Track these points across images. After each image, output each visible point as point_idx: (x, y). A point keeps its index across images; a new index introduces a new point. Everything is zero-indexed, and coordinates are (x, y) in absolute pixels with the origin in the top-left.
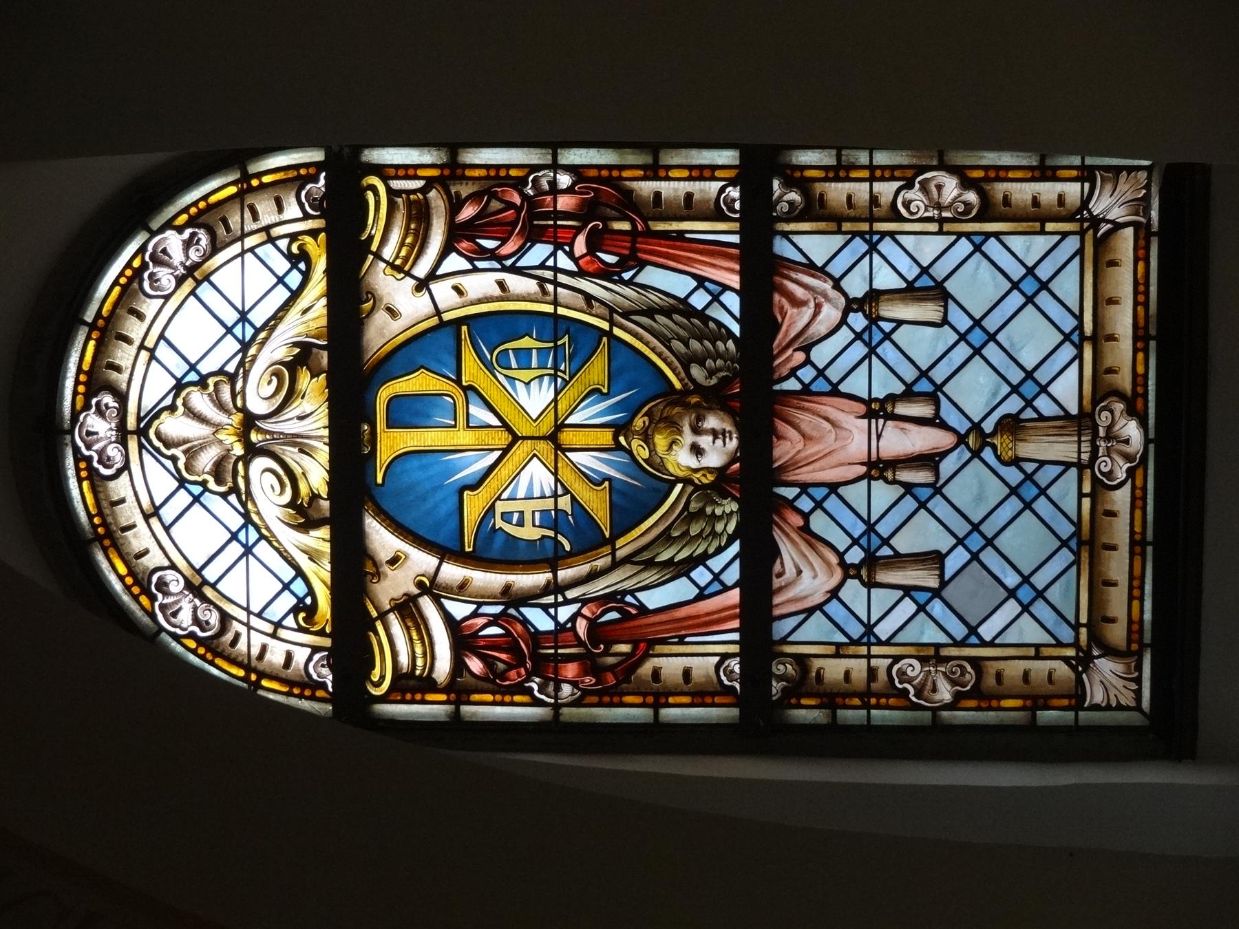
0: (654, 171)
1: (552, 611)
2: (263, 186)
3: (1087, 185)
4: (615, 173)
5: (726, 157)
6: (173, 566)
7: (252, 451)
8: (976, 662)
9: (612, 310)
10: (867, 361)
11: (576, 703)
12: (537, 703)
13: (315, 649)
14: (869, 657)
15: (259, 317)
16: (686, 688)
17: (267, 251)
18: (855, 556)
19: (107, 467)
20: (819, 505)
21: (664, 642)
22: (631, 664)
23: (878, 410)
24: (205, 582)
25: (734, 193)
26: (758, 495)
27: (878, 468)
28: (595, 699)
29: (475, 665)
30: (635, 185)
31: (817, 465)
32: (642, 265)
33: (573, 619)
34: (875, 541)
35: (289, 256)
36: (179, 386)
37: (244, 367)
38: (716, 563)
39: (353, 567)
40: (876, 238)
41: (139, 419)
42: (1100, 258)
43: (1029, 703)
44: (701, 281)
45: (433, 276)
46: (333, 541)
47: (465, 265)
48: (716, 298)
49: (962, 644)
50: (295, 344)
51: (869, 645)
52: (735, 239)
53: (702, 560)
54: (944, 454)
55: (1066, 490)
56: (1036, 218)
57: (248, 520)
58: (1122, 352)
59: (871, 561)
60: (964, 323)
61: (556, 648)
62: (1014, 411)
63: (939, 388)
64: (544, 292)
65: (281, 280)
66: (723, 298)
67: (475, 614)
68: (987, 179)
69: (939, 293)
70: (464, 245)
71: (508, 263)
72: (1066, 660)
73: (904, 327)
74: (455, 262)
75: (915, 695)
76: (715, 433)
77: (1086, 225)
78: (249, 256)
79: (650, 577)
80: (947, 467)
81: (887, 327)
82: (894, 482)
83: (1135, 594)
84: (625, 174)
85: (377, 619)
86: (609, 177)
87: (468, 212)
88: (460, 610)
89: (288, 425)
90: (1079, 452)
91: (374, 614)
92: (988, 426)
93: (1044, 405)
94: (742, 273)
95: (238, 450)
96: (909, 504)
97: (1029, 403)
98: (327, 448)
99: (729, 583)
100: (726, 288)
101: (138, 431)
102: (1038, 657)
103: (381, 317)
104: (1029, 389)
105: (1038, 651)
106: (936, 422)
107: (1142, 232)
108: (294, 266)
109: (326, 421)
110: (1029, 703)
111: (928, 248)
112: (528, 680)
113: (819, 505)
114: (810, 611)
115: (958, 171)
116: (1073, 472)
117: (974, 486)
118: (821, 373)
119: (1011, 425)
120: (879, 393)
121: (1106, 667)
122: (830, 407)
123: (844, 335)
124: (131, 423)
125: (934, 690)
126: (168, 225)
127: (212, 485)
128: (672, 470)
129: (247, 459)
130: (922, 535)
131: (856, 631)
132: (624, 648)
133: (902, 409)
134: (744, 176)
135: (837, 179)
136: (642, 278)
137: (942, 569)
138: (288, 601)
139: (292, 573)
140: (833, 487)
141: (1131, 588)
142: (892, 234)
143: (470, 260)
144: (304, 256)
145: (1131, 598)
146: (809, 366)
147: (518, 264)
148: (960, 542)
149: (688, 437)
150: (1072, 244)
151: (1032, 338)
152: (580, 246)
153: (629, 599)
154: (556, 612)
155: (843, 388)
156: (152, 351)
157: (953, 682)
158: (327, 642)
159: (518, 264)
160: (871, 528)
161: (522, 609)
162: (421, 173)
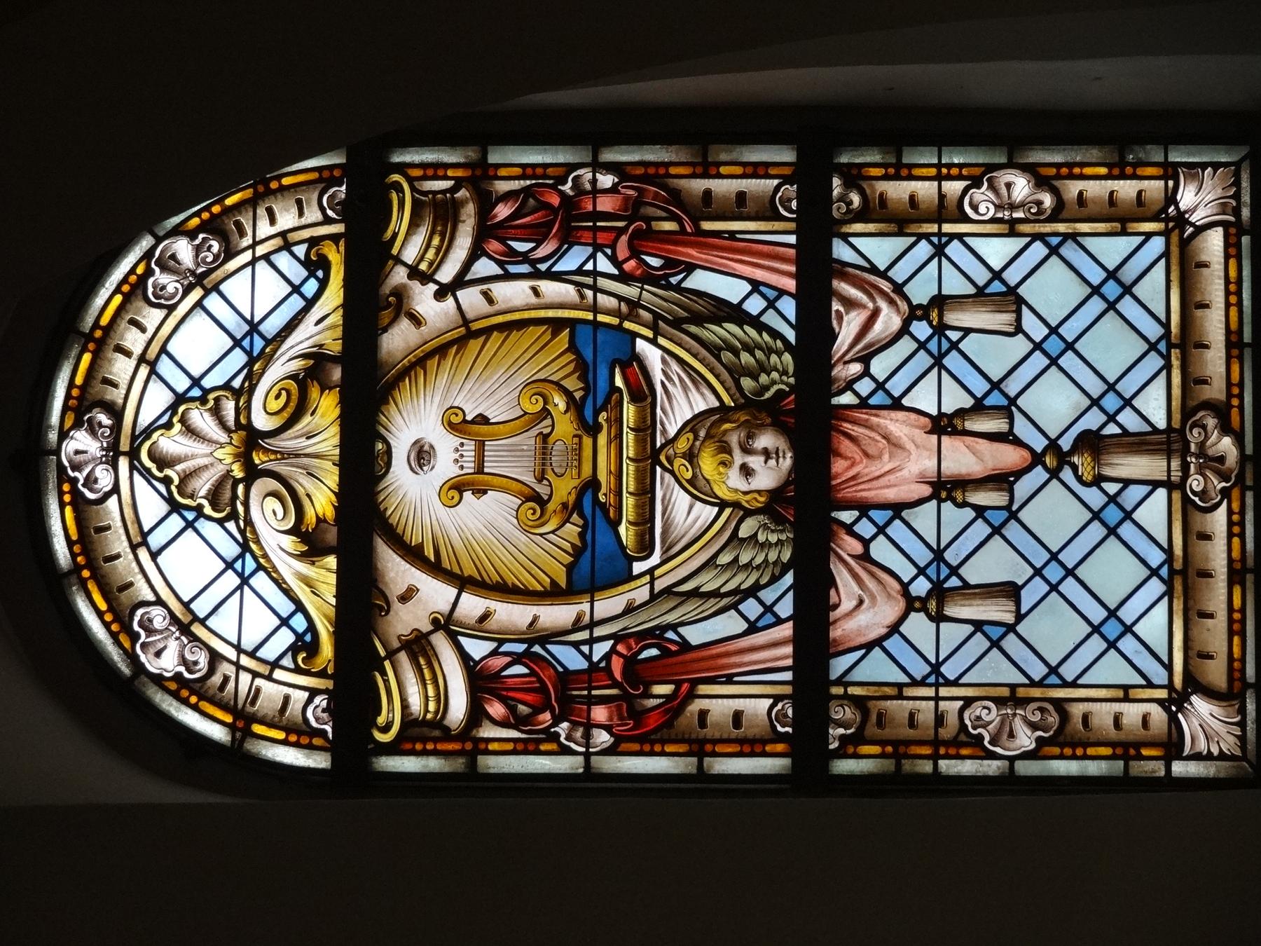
0: (707, 169)
1: (585, 649)
2: (282, 189)
3: (1171, 183)
4: (662, 171)
5: (786, 155)
6: (160, 602)
7: (253, 474)
8: (1059, 704)
9: (657, 317)
11: (610, 751)
13: (313, 692)
14: (937, 699)
15: (271, 327)
16: (735, 733)
17: (283, 260)
18: (921, 587)
19: (91, 490)
22: (676, 705)
23: (943, 425)
24: (195, 619)
25: (791, 190)
26: (810, 515)
30: (683, 183)
32: (690, 268)
33: (607, 657)
36: (180, 399)
37: (252, 380)
38: (768, 595)
39: (361, 600)
40: (932, 679)
41: (134, 437)
42: (1186, 268)
43: (1119, 751)
44: (756, 285)
45: (460, 281)
46: (341, 573)
47: (494, 269)
48: (771, 304)
49: (1040, 684)
50: (304, 356)
51: (937, 685)
52: (792, 239)
53: (753, 591)
55: (1154, 511)
56: (1120, 218)
57: (245, 547)
58: (1214, 361)
59: (939, 592)
60: (1037, 331)
61: (590, 689)
63: (1013, 401)
64: (582, 297)
65: (296, 289)
66: (779, 304)
67: (494, 653)
69: (1012, 300)
70: (494, 246)
72: (1159, 701)
74: (484, 267)
76: (766, 453)
77: (1171, 225)
78: (262, 267)
79: (690, 609)
80: (1023, 487)
81: (954, 336)
84: (673, 171)
85: (385, 659)
86: (655, 175)
87: (503, 211)
88: (477, 649)
90: (1169, 471)
91: (382, 653)
92: (1066, 443)
93: (1128, 419)
94: (797, 276)
95: (238, 473)
96: (981, 530)
97: (1112, 418)
98: (336, 470)
99: (783, 616)
100: (782, 292)
101: (126, 447)
102: (1126, 699)
104: (1111, 402)
105: (1126, 693)
108: (312, 274)
109: (336, 440)
111: (997, 251)
113: (881, 530)
114: (869, 647)
116: (1161, 493)
117: (1054, 511)
118: (880, 386)
119: (1091, 442)
120: (948, 408)
121: (1200, 705)
122: (895, 424)
124: (125, 445)
125: (1012, 735)
126: (177, 231)
127: (208, 510)
128: (719, 493)
129: (249, 480)
130: (994, 564)
132: (664, 689)
133: (971, 425)
136: (691, 283)
137: (1018, 604)
138: (285, 638)
139: (292, 607)
140: (898, 509)
141: (1231, 621)
142: (960, 237)
143: (500, 264)
144: (324, 264)
146: (867, 379)
147: (555, 269)
148: (1038, 572)
149: (739, 458)
150: (1157, 244)
151: (1112, 348)
152: (622, 251)
153: (670, 635)
155: (905, 402)
156: (153, 365)
157: (1034, 726)
158: (329, 684)
159: (555, 269)
160: (938, 555)
162: (450, 173)
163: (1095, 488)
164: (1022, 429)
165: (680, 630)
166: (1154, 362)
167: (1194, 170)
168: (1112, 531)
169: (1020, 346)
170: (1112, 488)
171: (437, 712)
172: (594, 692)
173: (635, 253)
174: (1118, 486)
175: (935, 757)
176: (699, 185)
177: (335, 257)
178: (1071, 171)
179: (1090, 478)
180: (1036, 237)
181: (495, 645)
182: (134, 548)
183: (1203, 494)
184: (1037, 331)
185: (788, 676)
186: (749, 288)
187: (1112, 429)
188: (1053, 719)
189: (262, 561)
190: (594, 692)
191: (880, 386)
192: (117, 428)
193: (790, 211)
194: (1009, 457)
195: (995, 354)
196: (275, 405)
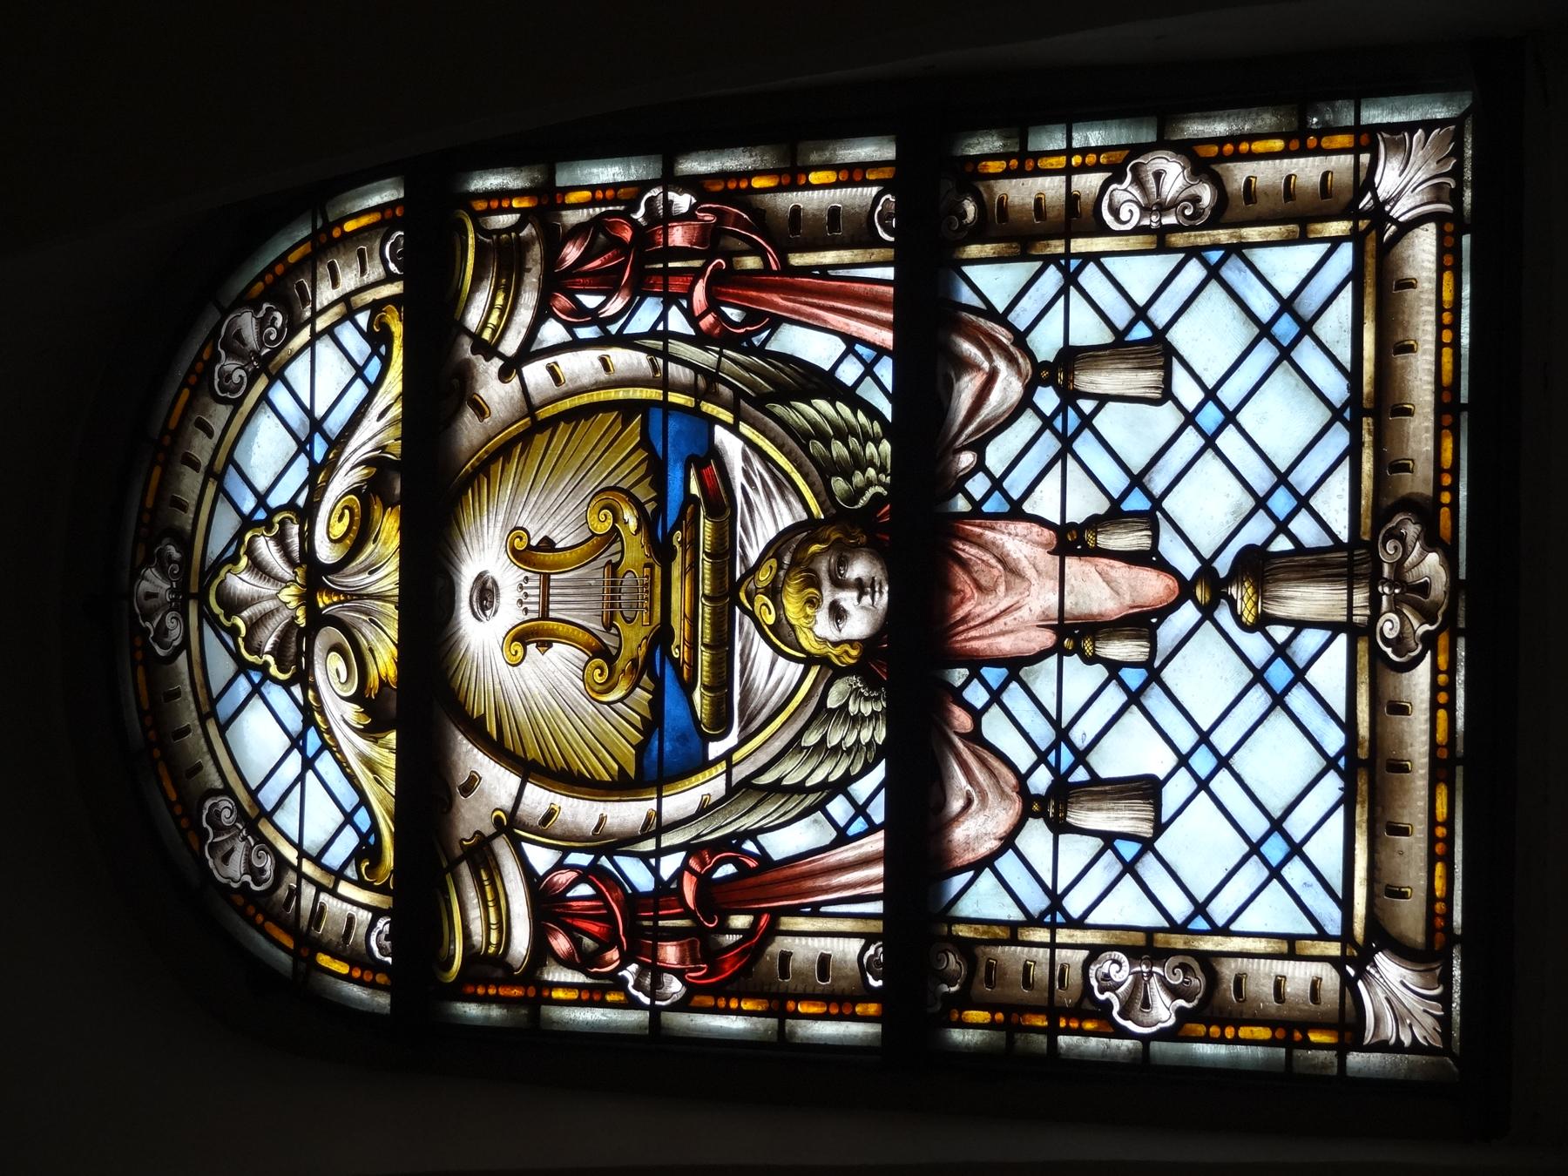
8: (1208, 960)
10: (1059, 465)
11: (683, 1005)
12: (633, 1004)
14: (1053, 946)
18: (1041, 781)
20: (996, 697)
21: (795, 911)
23: (1071, 541)
27: (1074, 634)
28: (709, 1001)
29: (561, 944)
31: (990, 629)
32: (775, 323)
33: (678, 876)
34: (1067, 758)
35: (368, 335)
38: (861, 789)
39: (426, 790)
40: (1074, 263)
44: (850, 341)
45: (528, 353)
46: (401, 752)
48: (869, 370)
51: (1053, 927)
52: (888, 273)
53: (840, 787)
54: (1165, 612)
56: (1298, 216)
57: (308, 722)
62: (1258, 540)
63: (1157, 503)
68: (1222, 158)
69: (1159, 352)
71: (613, 329)
73: (1111, 406)
75: (1120, 1014)
76: (860, 587)
77: (1363, 224)
80: (1169, 631)
81: (1087, 406)
82: (1090, 660)
83: (1438, 853)
88: (541, 858)
89: (356, 580)
92: (1223, 566)
94: (894, 326)
97: (1282, 527)
98: (395, 614)
100: (881, 351)
103: (469, 415)
105: (1290, 946)
106: (1150, 559)
107: (1449, 228)
110: (1280, 1034)
111: (1141, 274)
112: (623, 966)
115: (1186, 150)
117: (1206, 671)
119: (1257, 566)
120: (1077, 514)
121: (1390, 971)
123: (1027, 425)
127: (274, 670)
130: (1131, 751)
131: (1037, 902)
132: (741, 921)
134: (899, 179)
135: (1020, 173)
141: (1432, 839)
143: (569, 327)
145: (1432, 859)
151: (1284, 419)
153: (749, 846)
154: (658, 862)
157: (1174, 992)
161: (619, 860)
163: (1258, 634)
166: (1339, 439)
168: (1278, 700)
169: (1166, 419)
170: (1280, 633)
172: (661, 923)
173: (713, 304)
174: (1288, 630)
179: (1251, 619)
185: (877, 907)
187: (1282, 544)
188: (1198, 982)
190: (661, 923)
191: (997, 484)
193: (887, 230)
196: (339, 529)
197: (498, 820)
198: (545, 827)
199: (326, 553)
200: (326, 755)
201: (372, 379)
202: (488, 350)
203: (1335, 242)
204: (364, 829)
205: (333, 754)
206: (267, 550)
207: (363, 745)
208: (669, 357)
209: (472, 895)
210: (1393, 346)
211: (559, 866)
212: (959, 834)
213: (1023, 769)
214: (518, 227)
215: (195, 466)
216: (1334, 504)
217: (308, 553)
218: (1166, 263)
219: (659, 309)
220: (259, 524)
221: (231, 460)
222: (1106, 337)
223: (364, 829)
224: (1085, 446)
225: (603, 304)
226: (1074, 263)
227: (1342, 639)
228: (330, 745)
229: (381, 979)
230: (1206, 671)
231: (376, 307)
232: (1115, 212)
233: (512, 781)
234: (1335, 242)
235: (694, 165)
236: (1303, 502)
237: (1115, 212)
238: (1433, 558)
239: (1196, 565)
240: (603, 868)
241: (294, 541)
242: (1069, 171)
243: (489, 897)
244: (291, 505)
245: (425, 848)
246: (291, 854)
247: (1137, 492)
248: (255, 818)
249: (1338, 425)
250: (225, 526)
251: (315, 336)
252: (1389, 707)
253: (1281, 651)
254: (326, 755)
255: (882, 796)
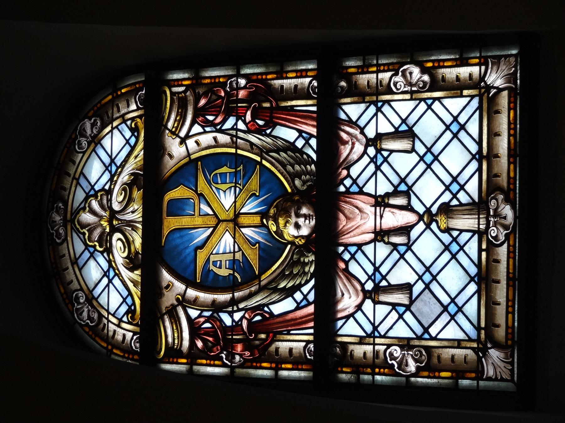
0: (281, 75)
3: (483, 68)
8: (428, 349)
11: (242, 366)
18: (369, 286)
20: (353, 257)
23: (381, 202)
27: (380, 235)
35: (131, 129)
38: (305, 289)
44: (300, 132)
45: (188, 136)
51: (375, 337)
52: (314, 109)
53: (298, 288)
56: (456, 88)
57: (110, 266)
59: (377, 289)
63: (410, 188)
69: (410, 134)
77: (483, 90)
80: (414, 233)
88: (194, 313)
90: (479, 224)
92: (434, 210)
94: (317, 127)
97: (455, 196)
98: (141, 227)
100: (311, 136)
103: (167, 157)
104: (455, 187)
106: (408, 208)
111: (404, 107)
121: (494, 353)
123: (366, 160)
127: (98, 248)
130: (402, 275)
133: (393, 201)
137: (411, 294)
138: (124, 308)
141: (507, 306)
143: (203, 127)
145: (507, 313)
151: (455, 158)
152: (248, 117)
153: (266, 309)
156: (78, 180)
157: (416, 361)
163: (446, 234)
164: (415, 203)
165: (270, 307)
166: (474, 165)
167: (497, 60)
168: (454, 256)
169: (414, 158)
170: (455, 234)
171: (178, 346)
172: (234, 337)
173: (254, 117)
174: (458, 232)
175: (373, 374)
176: (277, 83)
177: (141, 124)
178: (440, 64)
179: (443, 228)
180: (421, 100)
181: (199, 312)
182: (73, 265)
183: (496, 238)
184: (422, 150)
185: (311, 331)
186: (297, 134)
187: (455, 202)
188: (425, 357)
189: (117, 271)
190: (234, 337)
191: (355, 182)
192: (66, 209)
193: (314, 93)
194: (410, 218)
195: (403, 163)
196: (121, 198)
197: (177, 299)
198: (195, 303)
199: (116, 207)
200: (116, 278)
201: (132, 144)
202: (175, 134)
203: (472, 97)
204: (130, 304)
205: (119, 277)
206: (95, 205)
207: (130, 274)
208: (238, 137)
209: (168, 323)
210: (493, 134)
211: (200, 316)
212: (340, 306)
213: (363, 282)
214: (185, 92)
215: (69, 175)
216: (473, 187)
217: (111, 208)
218: (412, 104)
219: (235, 121)
220: (92, 196)
221: (82, 173)
222: (392, 130)
223: (130, 304)
224: (385, 167)
225: (215, 119)
226: (380, 104)
227: (476, 237)
228: (118, 275)
229: (136, 357)
230: (427, 246)
231: (133, 119)
232: (395, 84)
233: (183, 287)
234: (472, 97)
235: (247, 71)
236: (462, 187)
237: (395, 84)
238: (508, 207)
239: (424, 209)
240: (215, 317)
241: (105, 201)
242: (377, 72)
243: (175, 328)
244: (103, 189)
245: (150, 311)
246: (105, 314)
247: (403, 184)
248: (91, 299)
249: (474, 160)
250: (80, 195)
251: (113, 128)
252: (493, 261)
253: (455, 240)
254: (116, 278)
255: (313, 291)
